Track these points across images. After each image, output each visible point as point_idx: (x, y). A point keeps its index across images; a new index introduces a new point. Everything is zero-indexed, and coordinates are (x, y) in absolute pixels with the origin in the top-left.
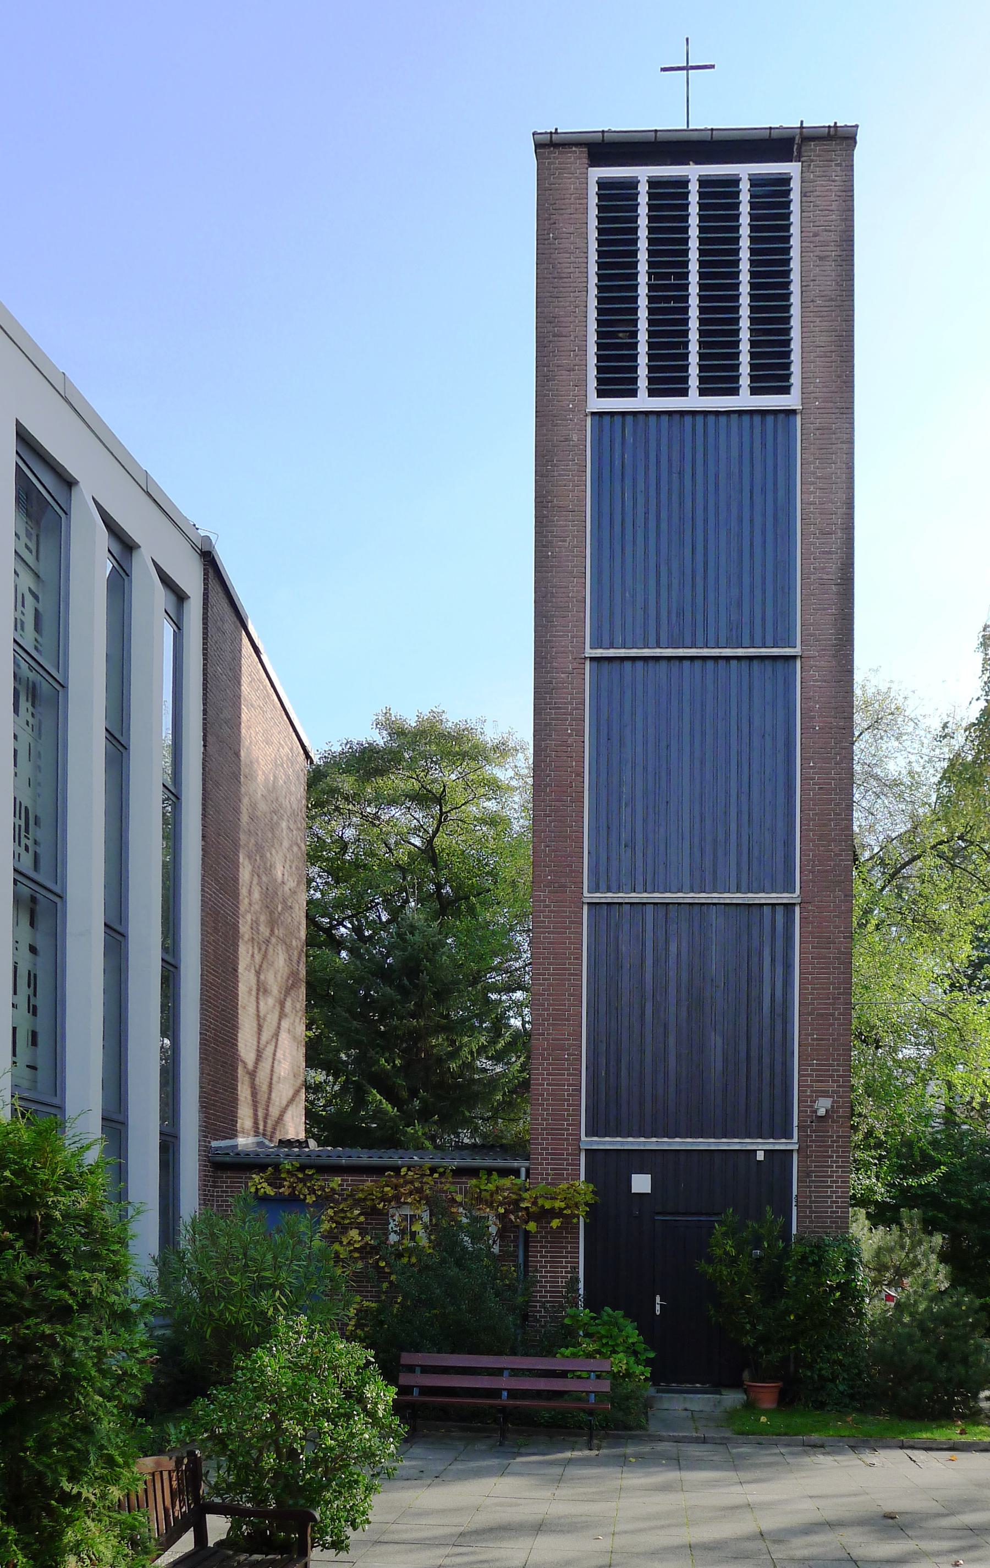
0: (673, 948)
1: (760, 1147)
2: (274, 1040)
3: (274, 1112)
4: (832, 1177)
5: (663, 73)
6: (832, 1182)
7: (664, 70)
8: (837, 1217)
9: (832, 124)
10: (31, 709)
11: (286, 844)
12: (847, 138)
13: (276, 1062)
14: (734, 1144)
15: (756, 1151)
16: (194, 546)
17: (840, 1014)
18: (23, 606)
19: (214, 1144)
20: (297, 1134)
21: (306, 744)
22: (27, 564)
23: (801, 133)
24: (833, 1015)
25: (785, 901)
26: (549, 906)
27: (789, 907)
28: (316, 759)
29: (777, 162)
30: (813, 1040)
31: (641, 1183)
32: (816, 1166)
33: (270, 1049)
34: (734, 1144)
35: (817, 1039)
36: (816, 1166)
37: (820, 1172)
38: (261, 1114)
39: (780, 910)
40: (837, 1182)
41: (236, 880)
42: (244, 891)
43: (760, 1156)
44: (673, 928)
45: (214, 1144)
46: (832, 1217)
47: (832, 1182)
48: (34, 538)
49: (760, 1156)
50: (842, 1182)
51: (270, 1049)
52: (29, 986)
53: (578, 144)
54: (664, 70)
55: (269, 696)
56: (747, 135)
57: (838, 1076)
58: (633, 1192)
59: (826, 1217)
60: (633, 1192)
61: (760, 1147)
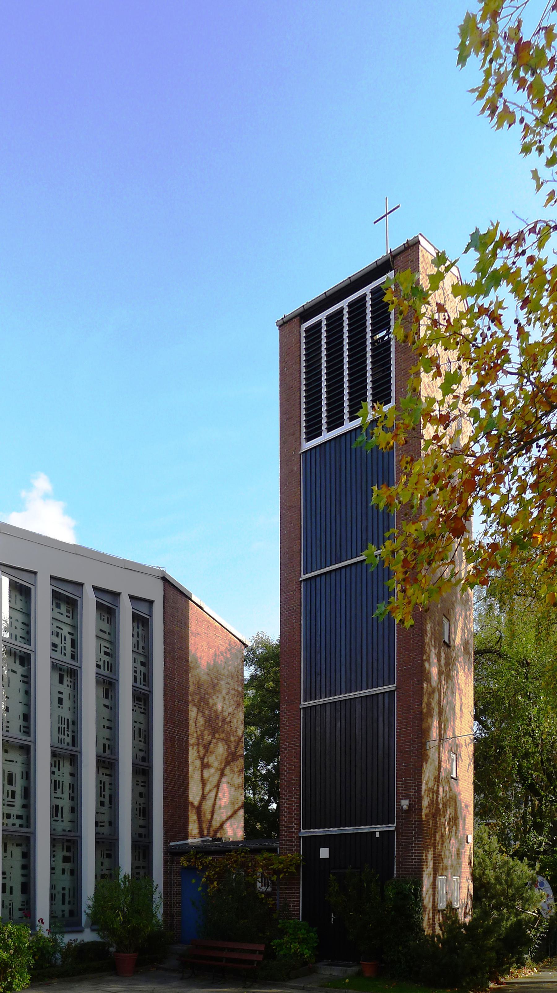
0: (338, 725)
1: (377, 830)
2: (215, 790)
3: (215, 824)
4: (412, 844)
5: (376, 224)
6: (412, 847)
7: (375, 223)
8: (415, 868)
9: (406, 242)
10: (69, 680)
11: (224, 692)
12: (416, 243)
13: (217, 800)
14: (365, 829)
15: (375, 832)
16: (157, 577)
17: (416, 750)
18: (65, 640)
19: (171, 844)
20: (235, 834)
21: (240, 638)
22: (65, 623)
23: (391, 255)
24: (412, 751)
25: (388, 690)
26: (286, 713)
27: (391, 693)
28: (250, 644)
29: (371, 283)
30: (403, 766)
31: (324, 853)
32: (404, 839)
33: (212, 794)
34: (365, 829)
35: (405, 766)
36: (404, 839)
37: (407, 842)
38: (205, 826)
39: (387, 695)
40: (415, 847)
41: (187, 719)
42: (191, 722)
43: (377, 835)
44: (338, 714)
45: (171, 844)
46: (412, 868)
47: (412, 847)
48: (71, 612)
49: (377, 835)
50: (418, 847)
51: (212, 794)
52: (70, 789)
53: (295, 317)
54: (375, 223)
55: (212, 625)
56: (366, 271)
57: (415, 786)
58: (321, 857)
59: (410, 868)
60: (321, 857)
61: (377, 830)
